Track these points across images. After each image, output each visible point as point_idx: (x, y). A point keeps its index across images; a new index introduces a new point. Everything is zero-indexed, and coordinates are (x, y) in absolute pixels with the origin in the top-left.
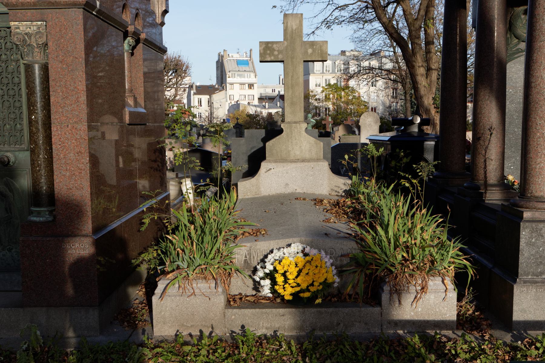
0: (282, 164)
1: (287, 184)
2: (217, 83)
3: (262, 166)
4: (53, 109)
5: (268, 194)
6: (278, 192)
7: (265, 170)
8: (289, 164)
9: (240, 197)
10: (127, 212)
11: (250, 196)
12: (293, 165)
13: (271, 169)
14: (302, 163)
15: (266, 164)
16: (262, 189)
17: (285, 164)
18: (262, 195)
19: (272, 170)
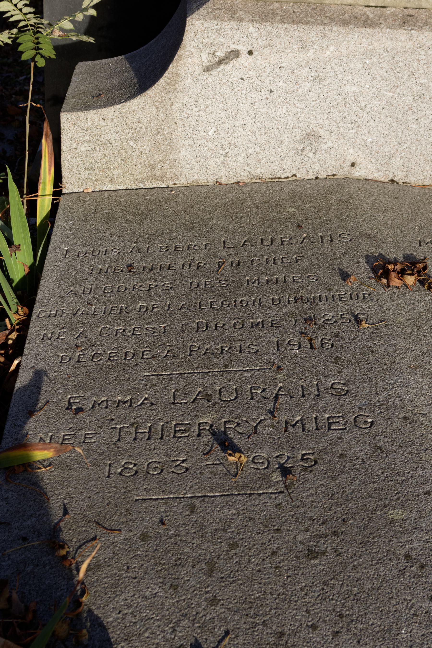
0: (297, 32)
1: (312, 137)
2: (63, 26)
3: (188, 36)
4: (65, 172)
5: (210, 180)
6: (265, 171)
7: (205, 59)
8: (337, 31)
9: (68, 186)
10: (23, 187)
11: (120, 180)
12: (356, 40)
13: (236, 54)
14: (402, 35)
15: (213, 25)
16: (185, 153)
17: (312, 33)
18: (184, 181)
19: (244, 60)
